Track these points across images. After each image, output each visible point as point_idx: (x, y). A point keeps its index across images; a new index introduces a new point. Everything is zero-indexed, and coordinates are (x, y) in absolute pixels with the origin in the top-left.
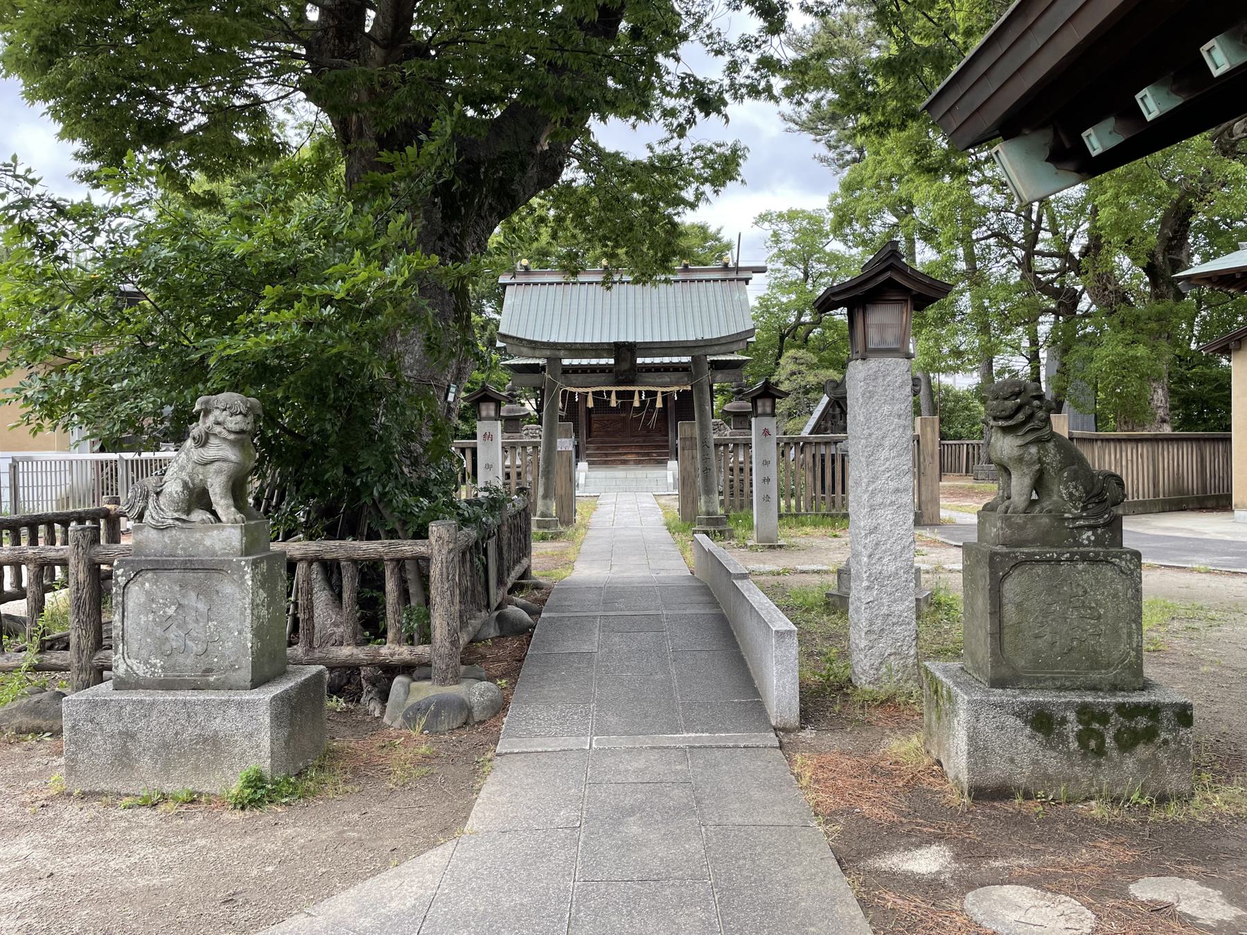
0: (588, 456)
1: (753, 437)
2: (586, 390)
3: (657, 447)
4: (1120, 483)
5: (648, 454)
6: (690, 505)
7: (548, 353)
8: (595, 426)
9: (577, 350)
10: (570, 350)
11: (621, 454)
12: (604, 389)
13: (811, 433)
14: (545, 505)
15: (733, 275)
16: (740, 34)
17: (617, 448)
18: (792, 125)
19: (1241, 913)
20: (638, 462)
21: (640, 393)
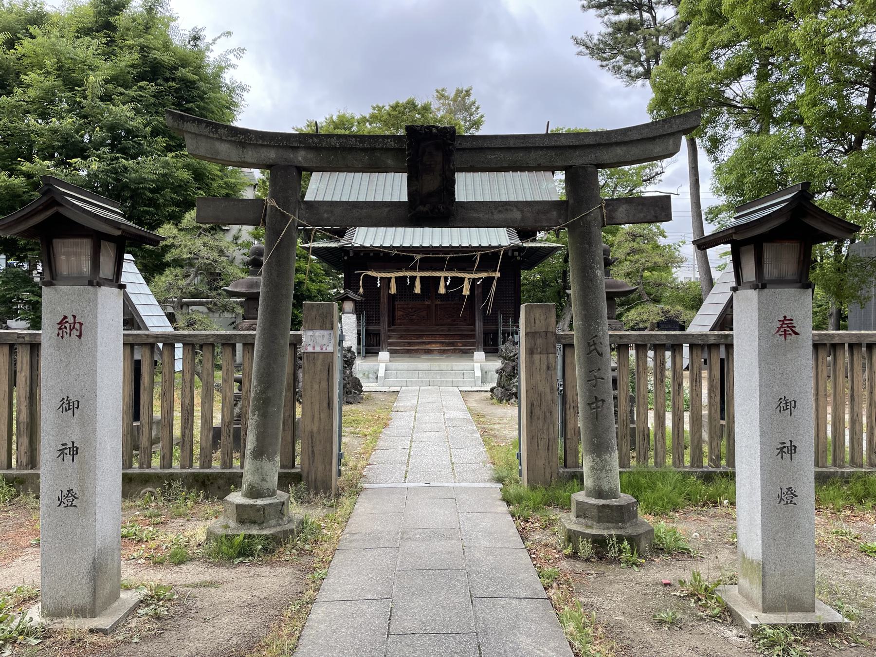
0: (391, 344)
5: (452, 344)
6: (543, 453)
7: (272, 155)
8: (399, 314)
9: (332, 149)
10: (316, 149)
13: (712, 329)
14: (257, 470)
17: (421, 336)
18: (582, 48)
20: (442, 352)
21: (446, 279)
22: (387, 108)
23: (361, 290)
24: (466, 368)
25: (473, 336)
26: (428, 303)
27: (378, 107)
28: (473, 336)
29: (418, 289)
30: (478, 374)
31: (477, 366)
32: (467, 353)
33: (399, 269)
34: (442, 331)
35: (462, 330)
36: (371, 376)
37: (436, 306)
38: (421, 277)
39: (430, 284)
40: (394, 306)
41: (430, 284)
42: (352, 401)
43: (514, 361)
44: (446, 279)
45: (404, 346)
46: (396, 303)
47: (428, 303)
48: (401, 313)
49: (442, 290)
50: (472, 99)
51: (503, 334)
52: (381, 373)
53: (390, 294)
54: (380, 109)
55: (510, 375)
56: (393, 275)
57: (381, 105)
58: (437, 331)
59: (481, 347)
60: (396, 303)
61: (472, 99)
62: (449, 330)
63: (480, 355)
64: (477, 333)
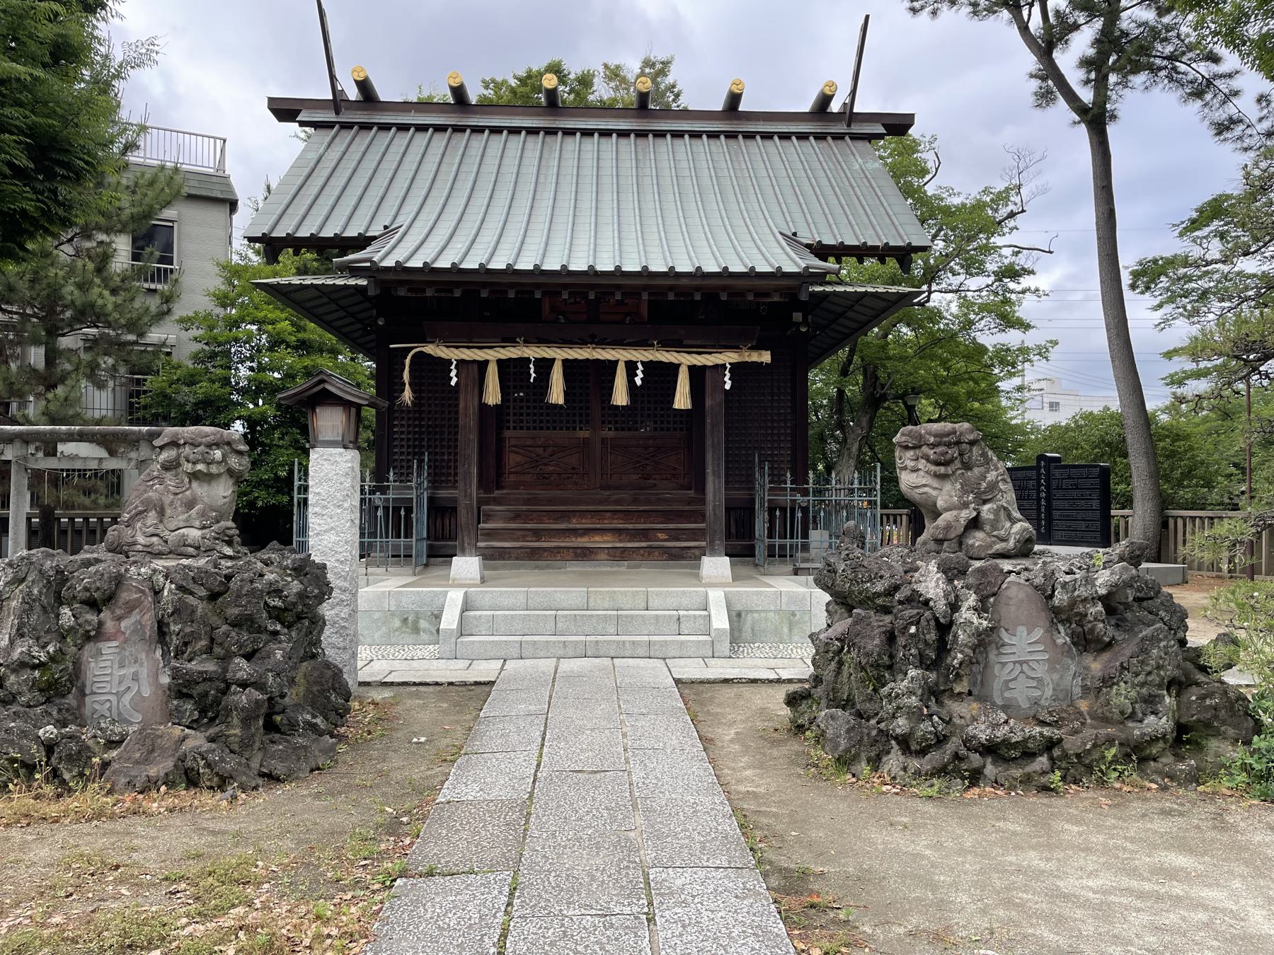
0: (490, 535)
2: (479, 355)
3: (668, 516)
5: (644, 534)
8: (512, 459)
11: (575, 532)
12: (533, 352)
15: (840, 128)
16: (1039, 111)
17: (565, 516)
20: (620, 555)
21: (631, 367)
22: (513, 83)
23: (407, 395)
24: (685, 602)
25: (701, 516)
26: (584, 434)
27: (493, 81)
28: (701, 516)
29: (557, 395)
30: (721, 621)
31: (716, 597)
32: (683, 557)
33: (509, 340)
34: (618, 502)
35: (667, 501)
36: (423, 624)
37: (604, 440)
39: (589, 380)
40: (500, 441)
41: (589, 380)
42: (279, 768)
43: (886, 610)
44: (631, 367)
45: (524, 539)
46: (507, 434)
47: (584, 434)
48: (519, 458)
49: (620, 397)
50: (670, 79)
51: (771, 511)
52: (450, 620)
53: (483, 407)
54: (498, 86)
55: (876, 666)
56: (492, 355)
57: (499, 79)
59: (720, 544)
60: (507, 434)
61: (670, 79)
62: (635, 501)
63: (716, 566)
64: (710, 507)
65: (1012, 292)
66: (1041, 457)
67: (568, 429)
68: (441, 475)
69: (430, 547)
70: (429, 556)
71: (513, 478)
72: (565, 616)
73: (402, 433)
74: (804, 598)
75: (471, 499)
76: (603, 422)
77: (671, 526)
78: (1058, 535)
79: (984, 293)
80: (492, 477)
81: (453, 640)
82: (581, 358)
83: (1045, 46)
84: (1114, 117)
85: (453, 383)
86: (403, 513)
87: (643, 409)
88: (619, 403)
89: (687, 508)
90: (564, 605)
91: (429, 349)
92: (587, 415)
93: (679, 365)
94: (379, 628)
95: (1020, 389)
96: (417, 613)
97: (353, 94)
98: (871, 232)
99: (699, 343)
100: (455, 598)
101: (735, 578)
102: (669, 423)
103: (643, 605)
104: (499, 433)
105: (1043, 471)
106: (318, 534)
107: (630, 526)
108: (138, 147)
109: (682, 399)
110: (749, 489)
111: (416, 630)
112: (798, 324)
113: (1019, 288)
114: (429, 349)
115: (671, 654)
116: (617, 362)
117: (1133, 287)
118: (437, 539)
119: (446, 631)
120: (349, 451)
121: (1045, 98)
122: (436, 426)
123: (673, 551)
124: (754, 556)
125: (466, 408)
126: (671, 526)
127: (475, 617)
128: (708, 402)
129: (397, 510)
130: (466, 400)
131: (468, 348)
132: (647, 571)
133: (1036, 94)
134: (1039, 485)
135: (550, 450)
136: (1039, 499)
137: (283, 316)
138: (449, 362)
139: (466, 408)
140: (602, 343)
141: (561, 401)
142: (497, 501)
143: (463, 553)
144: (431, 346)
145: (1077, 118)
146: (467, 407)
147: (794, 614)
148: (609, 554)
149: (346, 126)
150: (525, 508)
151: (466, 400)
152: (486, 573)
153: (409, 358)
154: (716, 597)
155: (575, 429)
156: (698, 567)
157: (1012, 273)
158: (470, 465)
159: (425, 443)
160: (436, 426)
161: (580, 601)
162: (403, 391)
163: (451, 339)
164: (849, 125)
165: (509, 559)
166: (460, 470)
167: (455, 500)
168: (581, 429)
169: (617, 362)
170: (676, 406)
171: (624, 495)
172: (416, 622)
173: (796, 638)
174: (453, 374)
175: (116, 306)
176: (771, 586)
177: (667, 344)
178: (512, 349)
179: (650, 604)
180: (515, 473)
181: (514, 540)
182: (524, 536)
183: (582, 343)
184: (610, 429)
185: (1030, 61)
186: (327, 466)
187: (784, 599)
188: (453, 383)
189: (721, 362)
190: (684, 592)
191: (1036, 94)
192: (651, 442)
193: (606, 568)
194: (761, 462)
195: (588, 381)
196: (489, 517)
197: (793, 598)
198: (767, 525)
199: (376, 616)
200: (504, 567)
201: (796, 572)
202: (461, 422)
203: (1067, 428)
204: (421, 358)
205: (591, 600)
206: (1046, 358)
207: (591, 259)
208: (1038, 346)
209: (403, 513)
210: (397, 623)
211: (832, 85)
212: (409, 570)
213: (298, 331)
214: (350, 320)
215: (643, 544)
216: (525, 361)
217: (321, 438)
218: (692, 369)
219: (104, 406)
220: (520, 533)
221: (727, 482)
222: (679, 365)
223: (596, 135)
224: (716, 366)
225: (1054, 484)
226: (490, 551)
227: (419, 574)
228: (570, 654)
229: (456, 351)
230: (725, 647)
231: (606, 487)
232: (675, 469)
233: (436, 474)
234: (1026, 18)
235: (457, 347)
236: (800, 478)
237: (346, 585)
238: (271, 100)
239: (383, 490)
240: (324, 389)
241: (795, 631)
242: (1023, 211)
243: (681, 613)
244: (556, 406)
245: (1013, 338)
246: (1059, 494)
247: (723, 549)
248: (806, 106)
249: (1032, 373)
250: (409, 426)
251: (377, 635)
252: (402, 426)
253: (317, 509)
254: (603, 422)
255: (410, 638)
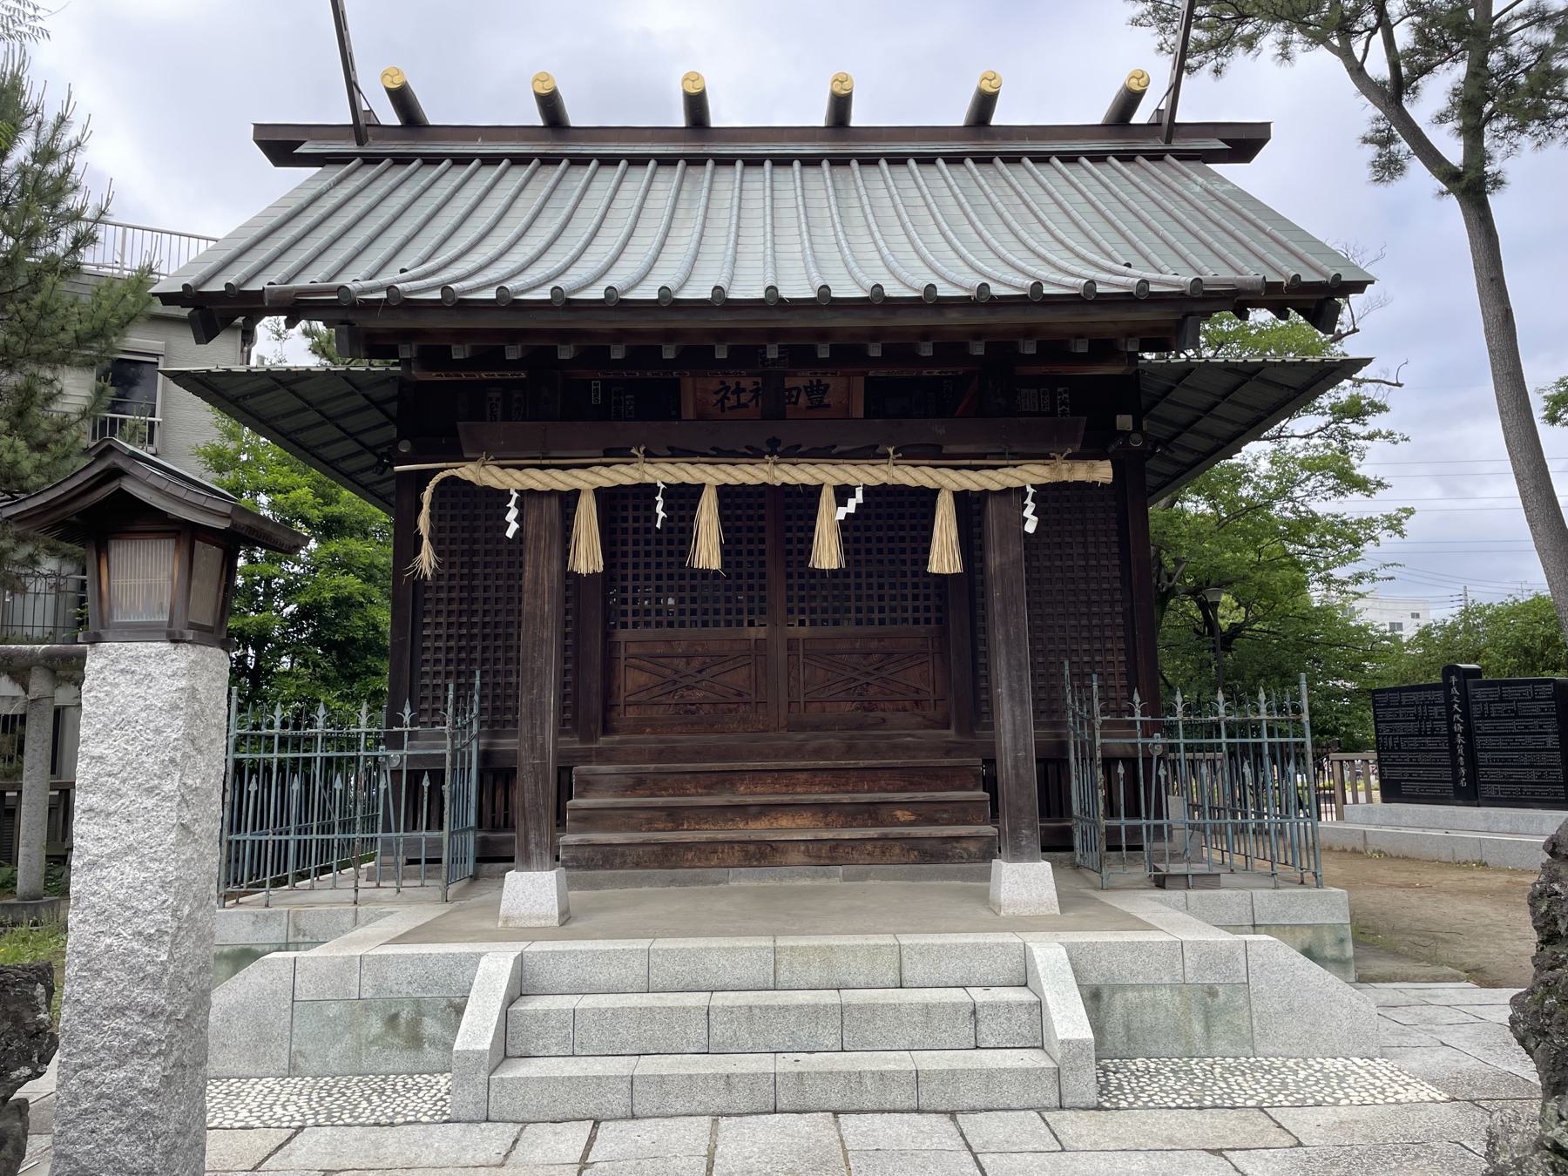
0: (590, 819)
1: (1190, 938)
2: (560, 480)
3: (913, 777)
4: (198, 342)
5: (871, 813)
8: (631, 680)
11: (741, 811)
12: (662, 473)
16: (1381, 187)
17: (725, 779)
19: (1548, 822)
20: (829, 854)
29: (707, 552)
30: (1070, 1022)
31: (1049, 956)
33: (617, 453)
34: (819, 753)
35: (906, 749)
36: (430, 1027)
37: (791, 644)
38: (724, 491)
40: (609, 649)
46: (622, 635)
48: (643, 678)
49: (827, 553)
52: (477, 1031)
53: (572, 580)
56: (586, 480)
58: (797, 751)
59: (1030, 837)
60: (622, 635)
62: (850, 750)
63: (1026, 881)
65: (1357, 437)
66: (1449, 670)
67: (728, 623)
68: (500, 713)
69: (483, 844)
70: (480, 860)
71: (632, 713)
72: (729, 1010)
73: (438, 637)
74: (1231, 956)
75: (543, 756)
76: (790, 611)
77: (920, 796)
78: (1491, 791)
79: (1316, 441)
80: (591, 709)
81: (483, 1075)
82: (752, 481)
83: (1391, 96)
84: (1498, 183)
85: (510, 534)
86: (426, 783)
87: (859, 586)
88: (825, 565)
89: (946, 762)
90: (727, 979)
91: (468, 472)
92: (762, 599)
93: (936, 492)
94: (336, 1038)
95: (1358, 579)
96: (417, 1002)
97: (388, 116)
98: (1258, 264)
99: (971, 449)
100: (494, 968)
101: (1067, 901)
102: (905, 610)
103: (892, 976)
104: (607, 635)
105: (1454, 691)
106: (92, 865)
107: (845, 798)
108: (95, 241)
109: (944, 557)
110: (1055, 725)
111: (415, 1041)
112: (1126, 434)
113: (1363, 431)
114: (468, 472)
115: (968, 1101)
116: (818, 489)
117: (1553, 419)
118: (494, 828)
119: (465, 1056)
120: (184, 649)
121: (1389, 168)
122: (497, 625)
123: (927, 845)
124: (1071, 848)
125: (536, 581)
126: (920, 796)
127: (535, 1016)
128: (994, 560)
129: (415, 777)
130: (536, 567)
131: (542, 467)
132: (884, 888)
133: (1373, 164)
134: (1450, 712)
135: (696, 663)
136: (1452, 735)
137: (303, 480)
138: (505, 495)
139: (536, 581)
140: (793, 453)
141: (716, 564)
142: (604, 756)
143: (527, 864)
144: (471, 466)
145: (1445, 188)
146: (538, 577)
147: (1212, 993)
148: (807, 853)
149: (371, 160)
150: (652, 766)
151: (536, 567)
152: (574, 894)
153: (432, 484)
154: (1049, 956)
155: (740, 624)
156: (986, 876)
157: (1355, 410)
158: (542, 689)
159: (477, 655)
160: (497, 625)
161: (762, 972)
162: (418, 551)
163: (507, 456)
164: (1168, 141)
165: (622, 866)
166: (524, 699)
167: (514, 755)
168: (751, 624)
169: (818, 489)
170: (934, 567)
171: (833, 740)
172: (415, 1023)
173: (1221, 1045)
174: (511, 516)
175: (38, 468)
176: (1148, 927)
177: (912, 453)
178: (623, 468)
179: (907, 974)
180: (637, 704)
181: (637, 828)
182: (650, 821)
183: (754, 454)
184: (802, 623)
185: (1366, 114)
186: (125, 687)
187: (1191, 959)
188: (510, 534)
189: (1016, 484)
190: (976, 947)
191: (1373, 164)
192: (874, 645)
193: (804, 880)
194: (1081, 677)
195: (762, 541)
196: (588, 786)
197: (1210, 958)
198: (1101, 793)
199: (333, 1010)
200: (612, 883)
201: (1160, 882)
202: (526, 608)
203: (1453, 630)
204: (453, 485)
205: (782, 969)
206: (1401, 533)
207: (770, 274)
208: (1388, 518)
209: (426, 783)
210: (376, 1026)
211: (1141, 75)
212: (434, 887)
213: (326, 504)
214: (351, 446)
215: (872, 832)
216: (646, 492)
217: (118, 618)
218: (963, 499)
219: (38, 622)
220: (643, 815)
221: (1037, 712)
222: (936, 492)
223: (768, 164)
224: (1007, 492)
225: (1475, 710)
226: (588, 852)
227: (460, 895)
228: (742, 1107)
229: (517, 474)
230: (1084, 1085)
231: (793, 727)
232: (917, 691)
233: (495, 709)
234: (1359, 56)
235: (520, 468)
236: (1156, 705)
237: (159, 998)
238: (259, 128)
239: (395, 741)
240: (121, 491)
241: (1219, 1029)
242: (1355, 330)
243: (979, 995)
244: (705, 573)
245: (1353, 506)
246: (1485, 726)
247: (1037, 846)
248: (1097, 114)
249: (1378, 551)
250: (450, 625)
251: (333, 1053)
252: (438, 625)
253: (94, 800)
254: (790, 611)
255: (401, 1060)
